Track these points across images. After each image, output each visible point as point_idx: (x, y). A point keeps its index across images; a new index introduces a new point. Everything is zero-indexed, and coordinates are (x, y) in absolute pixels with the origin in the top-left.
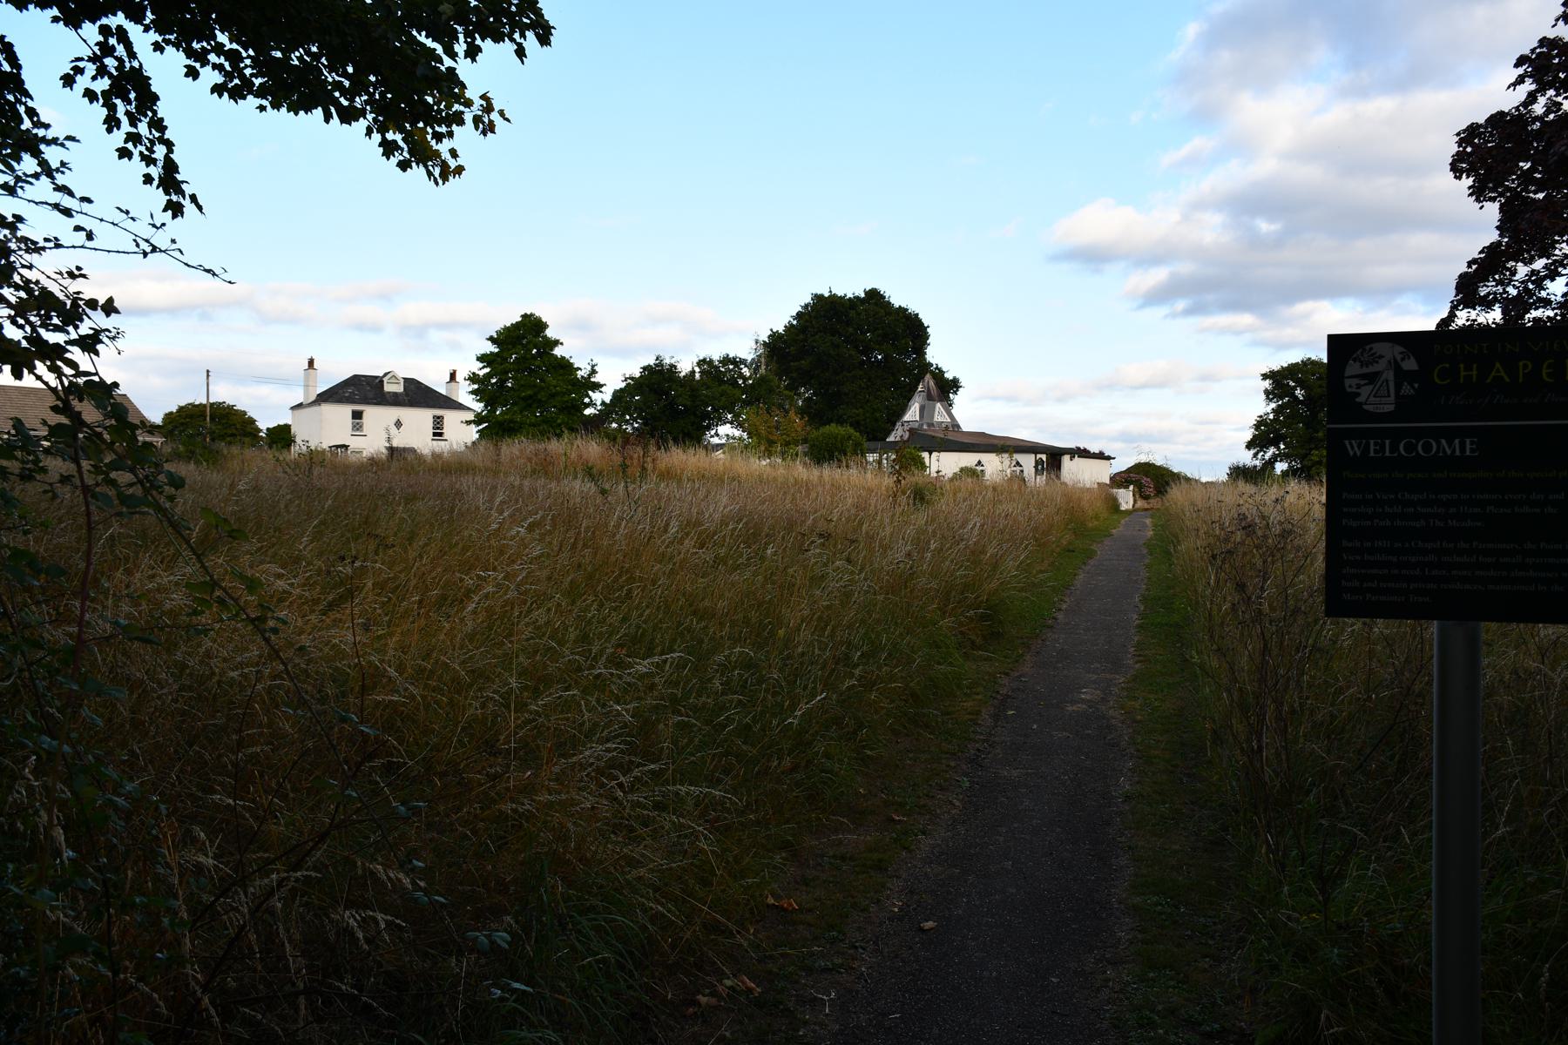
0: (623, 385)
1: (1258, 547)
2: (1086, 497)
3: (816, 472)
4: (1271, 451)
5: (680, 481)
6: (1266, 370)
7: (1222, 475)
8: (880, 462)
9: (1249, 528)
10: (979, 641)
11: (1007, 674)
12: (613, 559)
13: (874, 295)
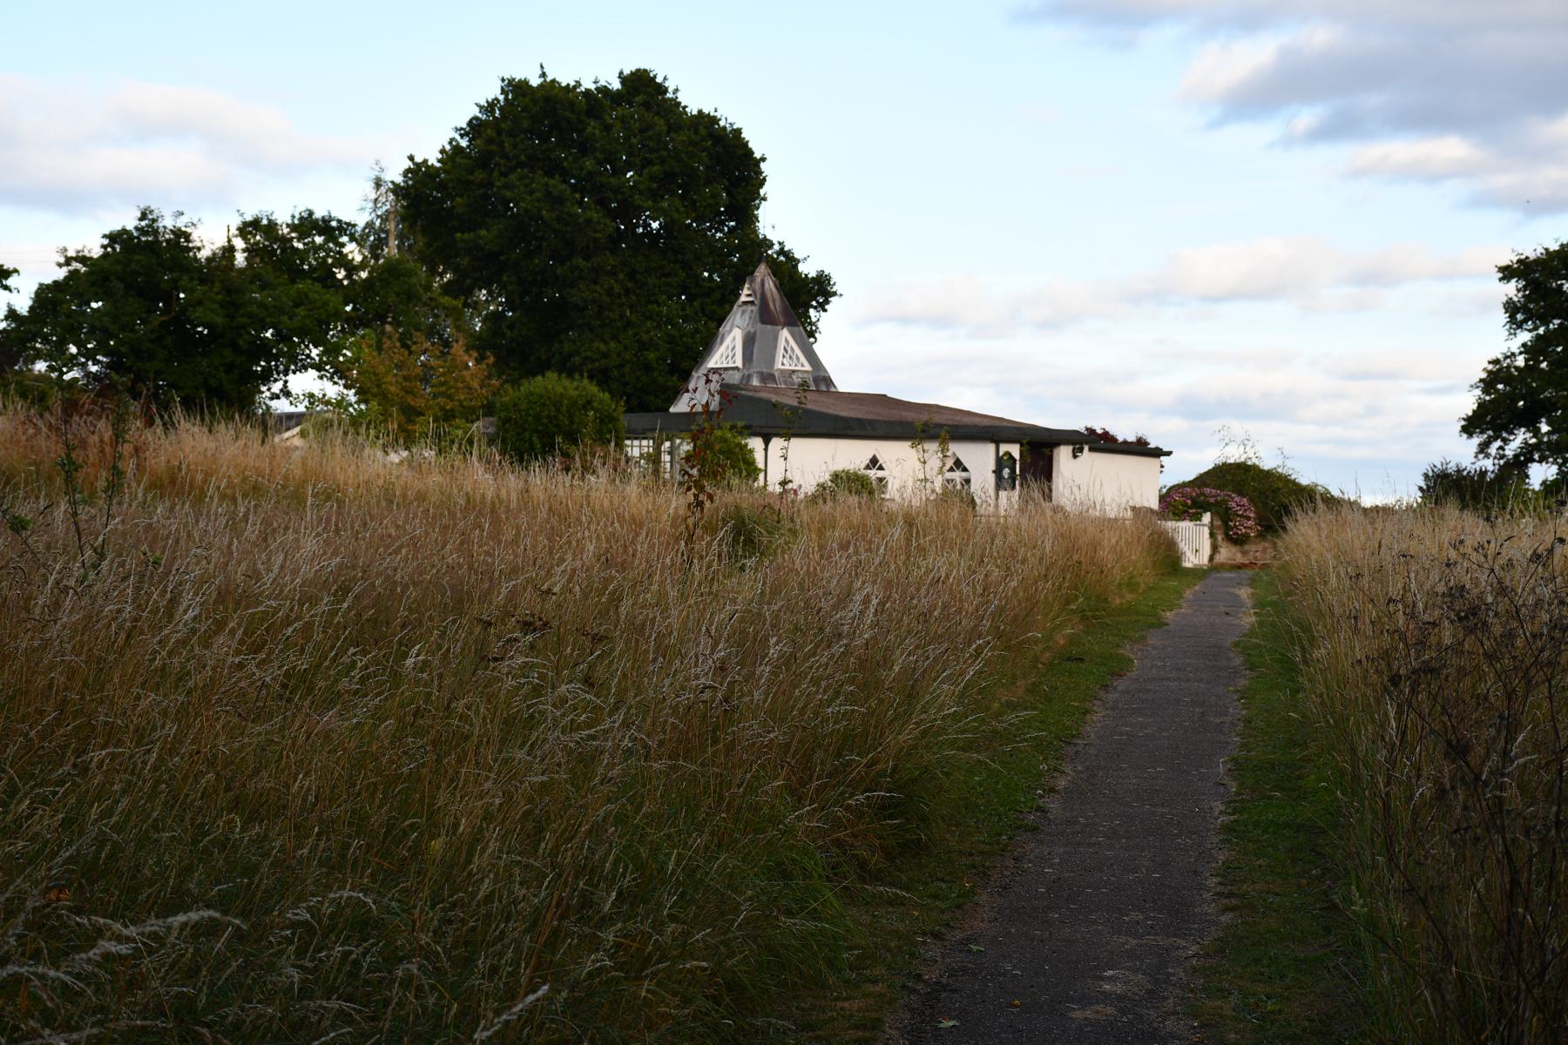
0: (61, 274)
1: (1491, 657)
2: (1110, 539)
3: (513, 482)
4: (1519, 439)
5: (199, 500)
6: (1508, 258)
7: (1406, 491)
8: (655, 459)
9: (1470, 616)
10: (876, 860)
11: (937, 936)
12: (41, 682)
13: (641, 85)
